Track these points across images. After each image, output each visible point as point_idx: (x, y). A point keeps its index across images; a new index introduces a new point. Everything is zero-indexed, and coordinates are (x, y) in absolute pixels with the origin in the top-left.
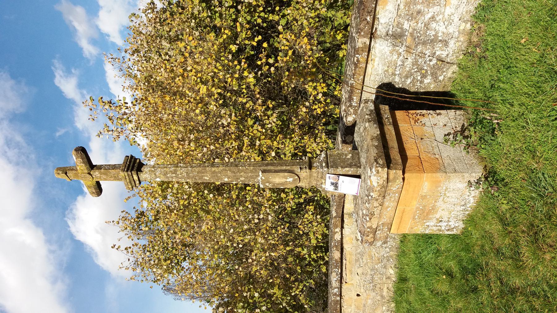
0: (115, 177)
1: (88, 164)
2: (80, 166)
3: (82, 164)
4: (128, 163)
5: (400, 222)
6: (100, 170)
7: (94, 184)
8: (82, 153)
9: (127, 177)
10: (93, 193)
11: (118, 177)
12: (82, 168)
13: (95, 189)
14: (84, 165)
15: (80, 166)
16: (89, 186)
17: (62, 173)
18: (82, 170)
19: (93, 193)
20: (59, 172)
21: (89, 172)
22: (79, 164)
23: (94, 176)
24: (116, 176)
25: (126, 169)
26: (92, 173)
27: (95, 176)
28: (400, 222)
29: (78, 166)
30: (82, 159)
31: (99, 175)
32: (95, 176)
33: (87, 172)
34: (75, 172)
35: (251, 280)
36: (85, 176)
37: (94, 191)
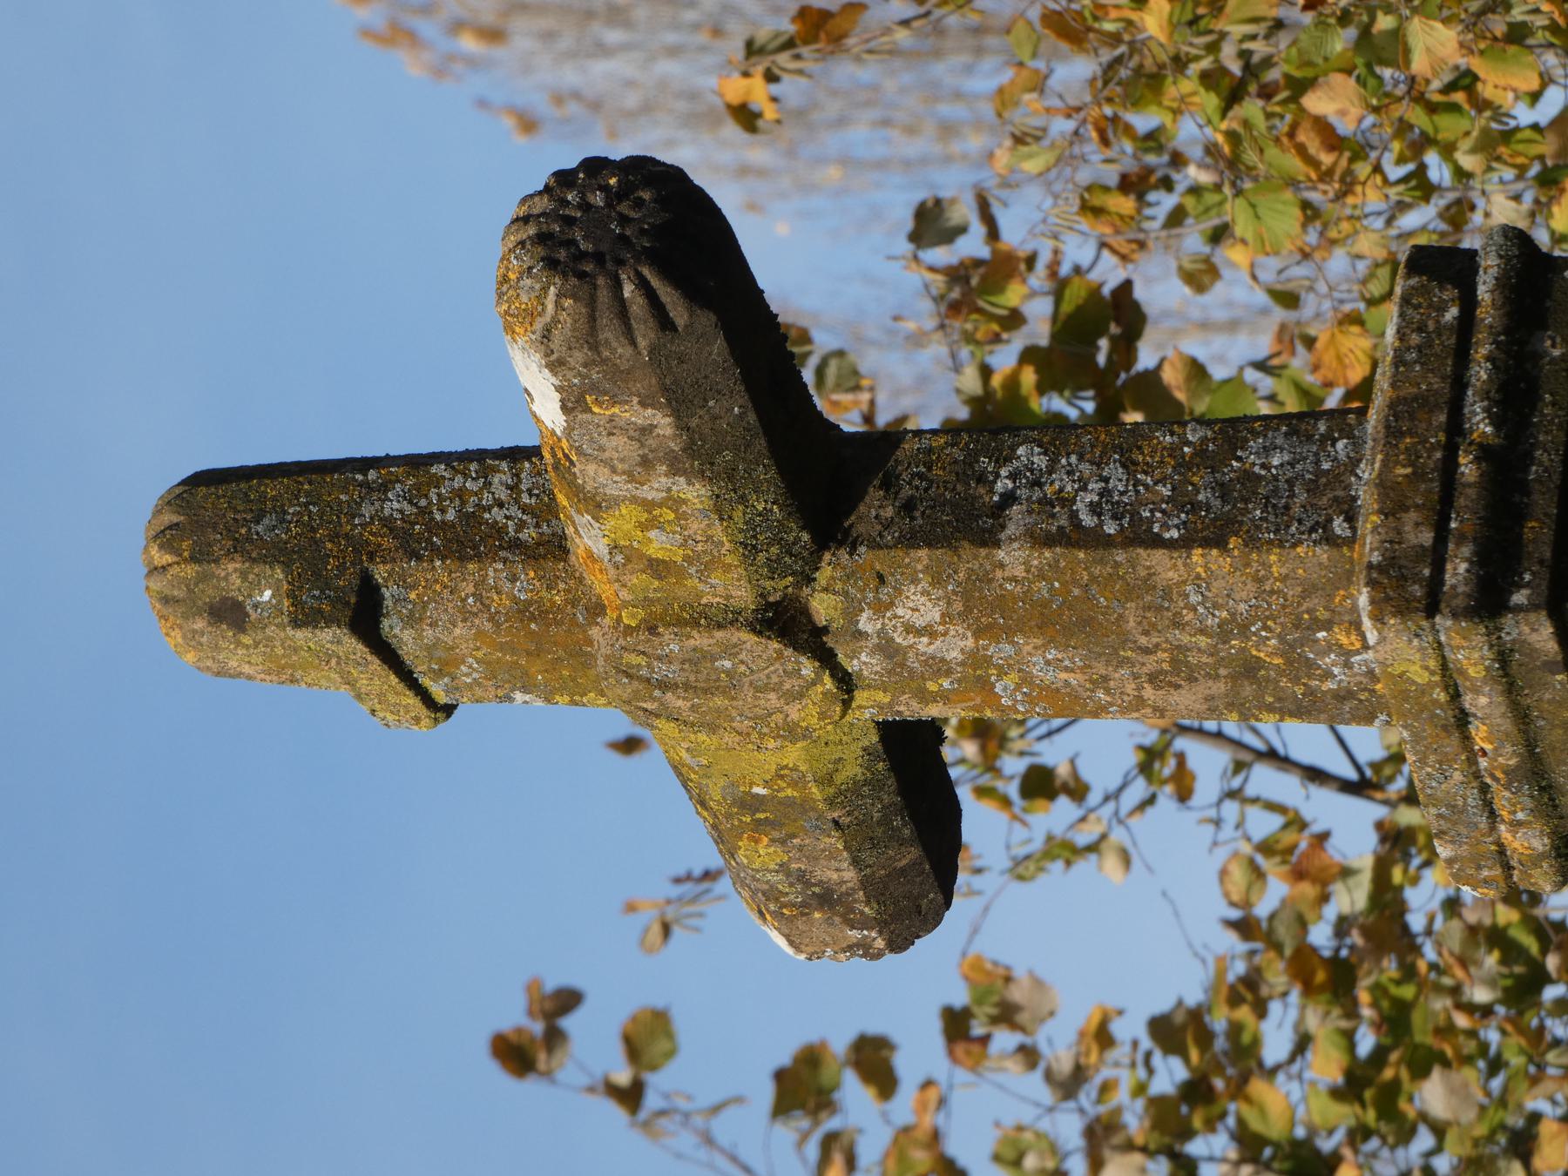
0: (1249, 669)
1: (766, 473)
2: (625, 520)
3: (658, 485)
4: (1481, 425)
5: (1176, 914)
6: (971, 560)
7: (852, 770)
8: (679, 313)
9: (1483, 702)
10: (827, 899)
11: (1298, 665)
12: (659, 544)
13: (859, 838)
14: (695, 493)
15: (625, 520)
16: (751, 804)
17: (304, 617)
18: (657, 568)
19: (827, 899)
20: (231, 575)
21: (779, 587)
22: (616, 487)
23: (863, 662)
24: (1268, 651)
25: (1458, 570)
26: (823, 607)
27: (887, 648)
28: (1176, 914)
29: (596, 505)
30: (678, 401)
31: (956, 645)
32: (887, 648)
33: (743, 596)
34: (525, 585)
35: (1190, 488)
36: (697, 659)
37: (841, 873)
